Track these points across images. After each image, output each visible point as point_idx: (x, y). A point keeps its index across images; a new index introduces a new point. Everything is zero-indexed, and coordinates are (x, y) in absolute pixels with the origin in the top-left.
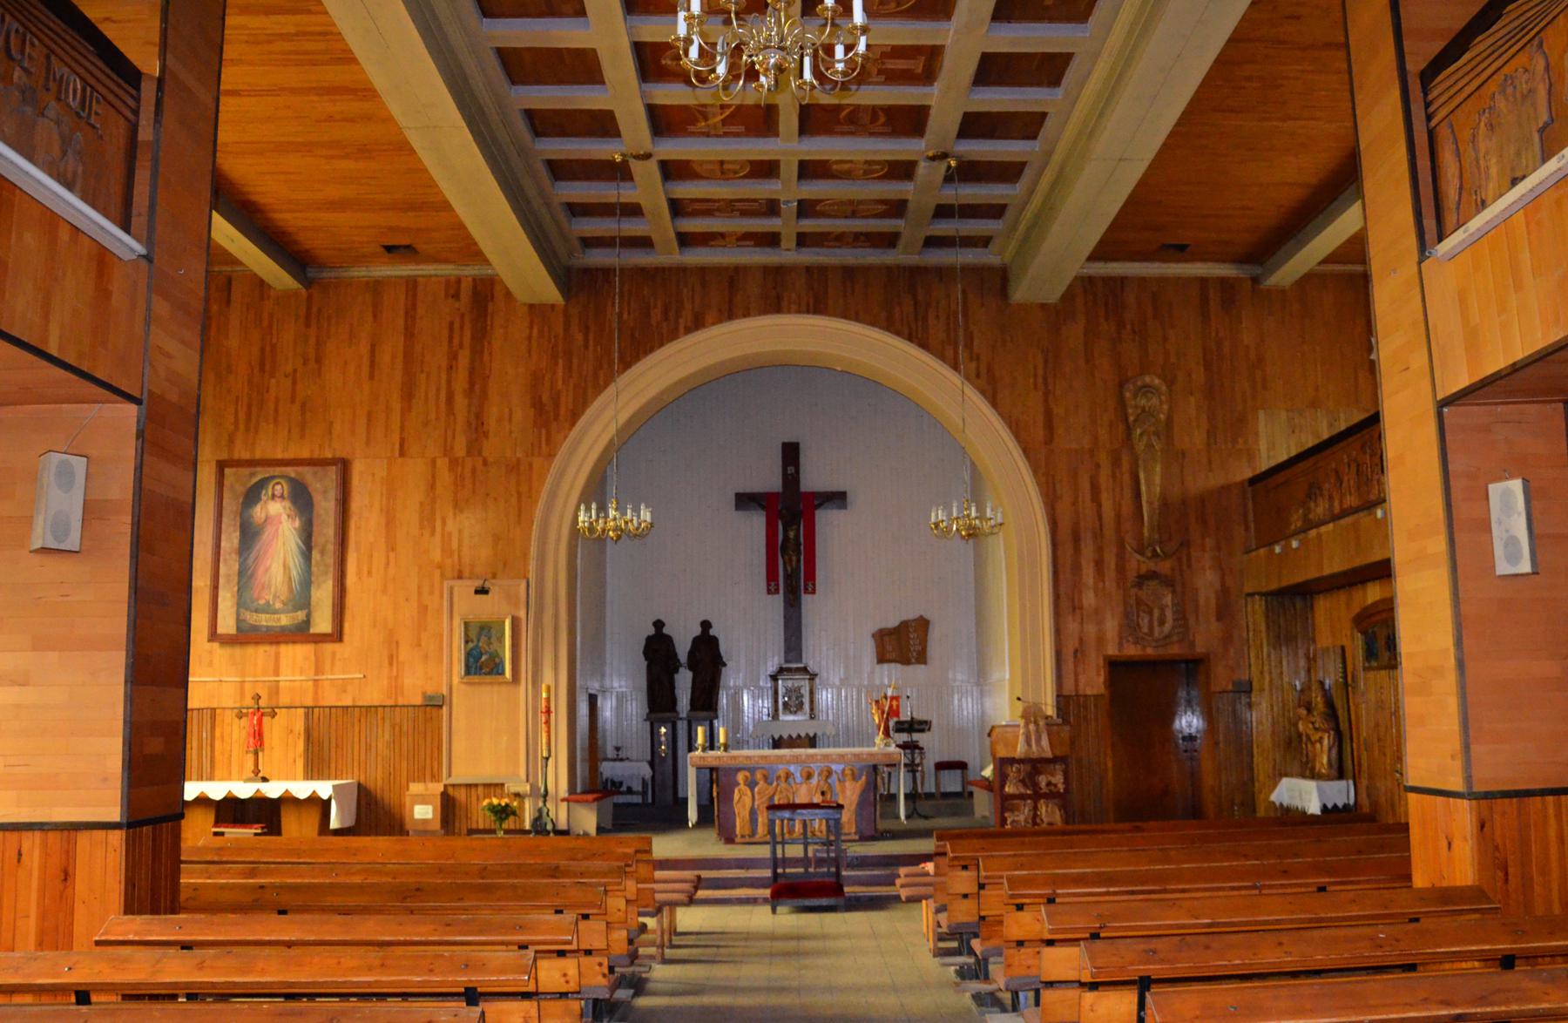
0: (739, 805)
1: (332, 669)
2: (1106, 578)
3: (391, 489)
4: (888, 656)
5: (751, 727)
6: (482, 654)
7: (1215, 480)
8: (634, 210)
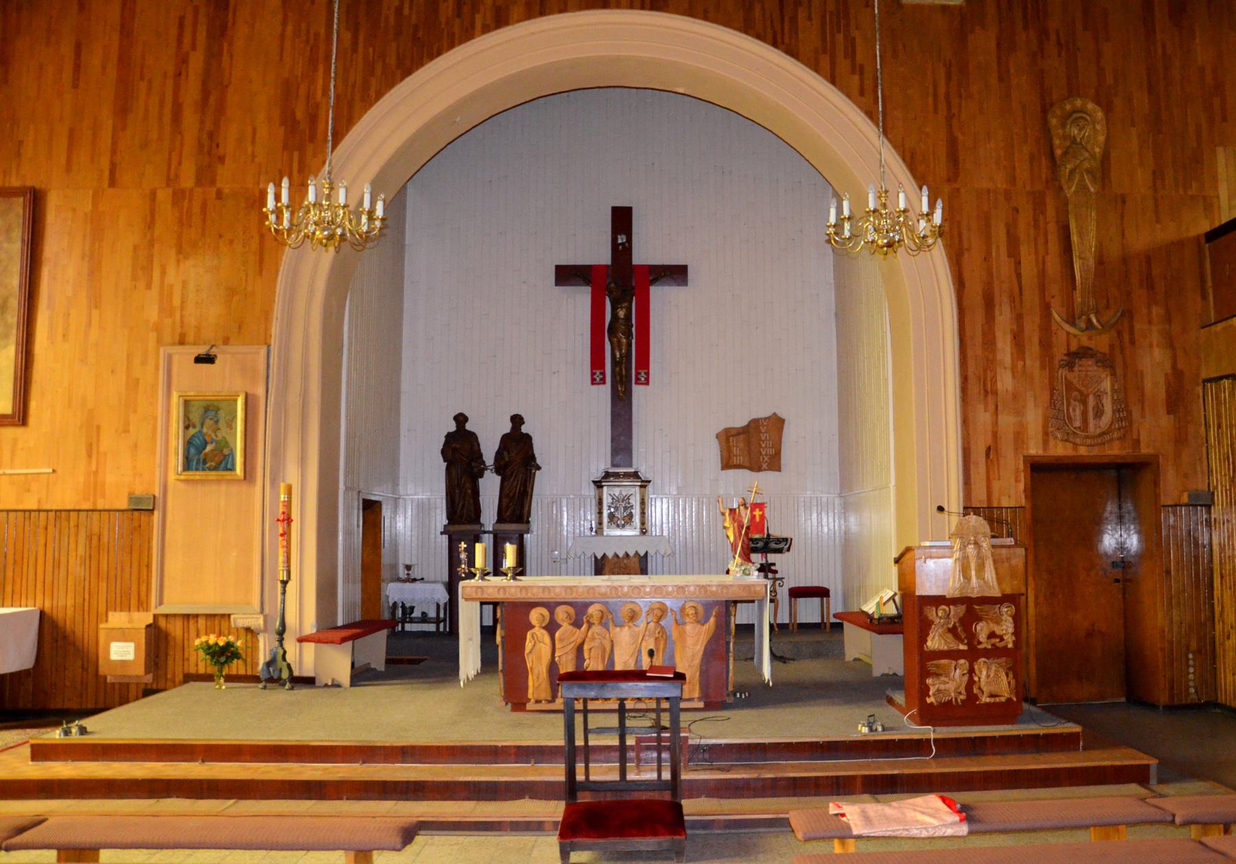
0: (530, 656)
1: (12, 459)
2: (1027, 354)
3: (96, 227)
4: (735, 461)
6: (206, 443)
7: (1167, 233)
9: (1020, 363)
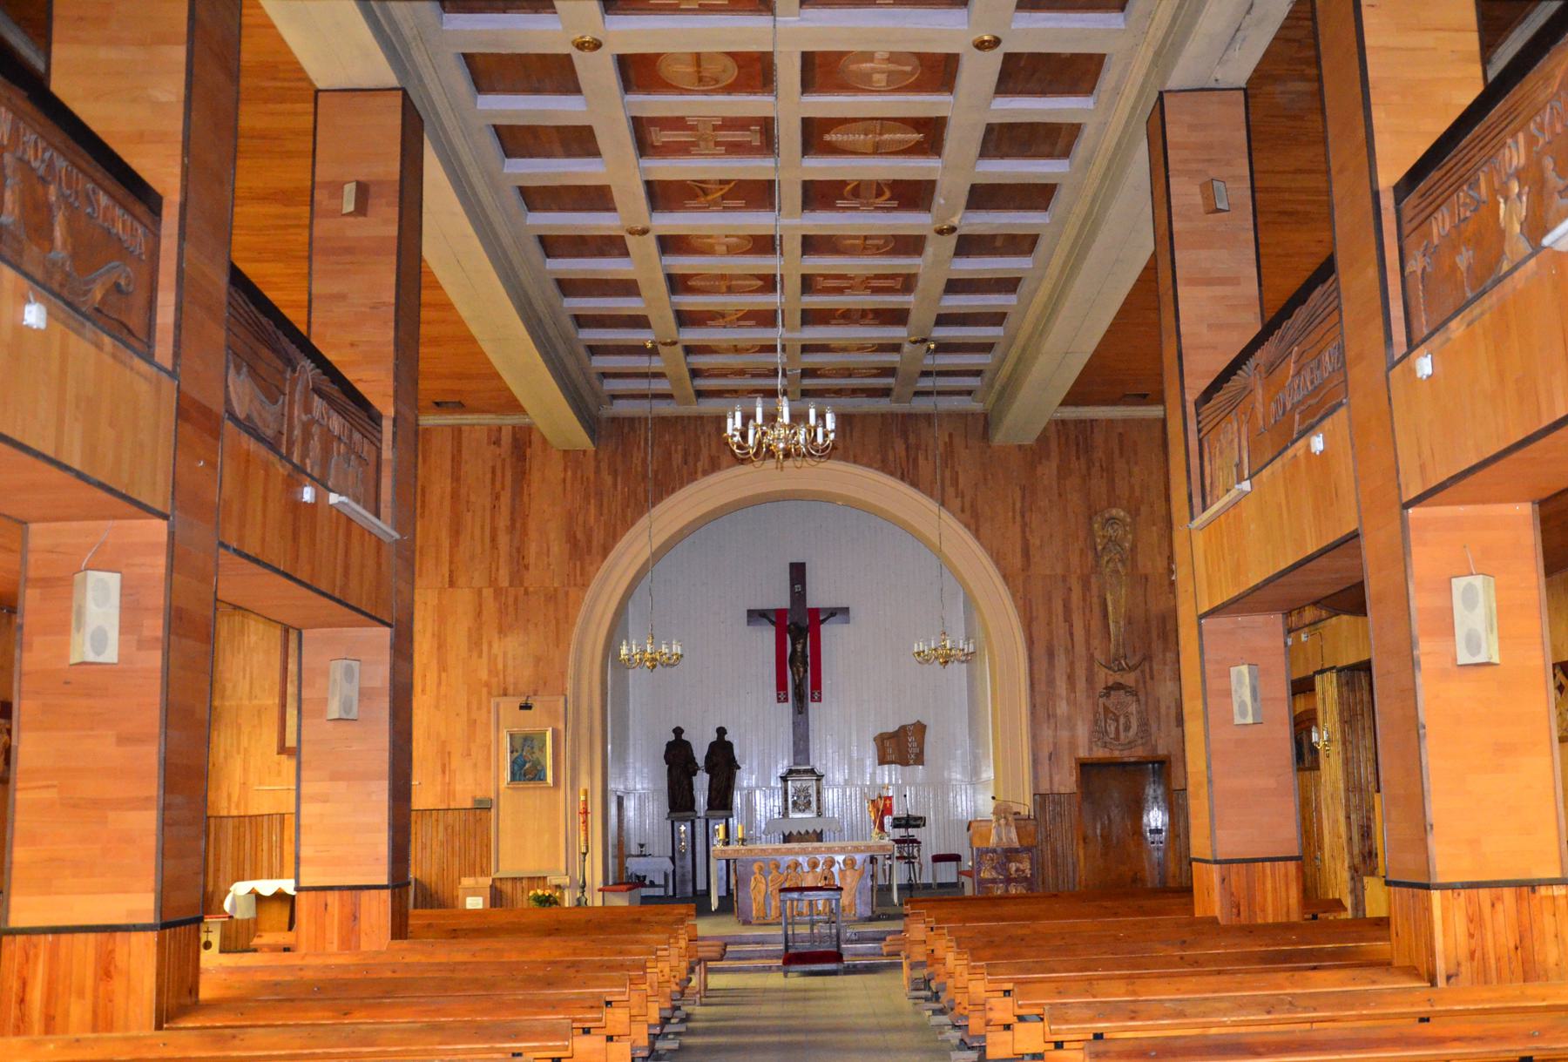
0: (755, 891)
4: (888, 758)
5: (763, 826)
6: (525, 763)
8: (628, 288)
9: (1072, 695)
